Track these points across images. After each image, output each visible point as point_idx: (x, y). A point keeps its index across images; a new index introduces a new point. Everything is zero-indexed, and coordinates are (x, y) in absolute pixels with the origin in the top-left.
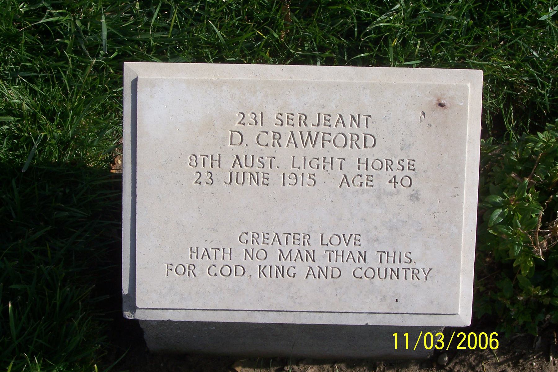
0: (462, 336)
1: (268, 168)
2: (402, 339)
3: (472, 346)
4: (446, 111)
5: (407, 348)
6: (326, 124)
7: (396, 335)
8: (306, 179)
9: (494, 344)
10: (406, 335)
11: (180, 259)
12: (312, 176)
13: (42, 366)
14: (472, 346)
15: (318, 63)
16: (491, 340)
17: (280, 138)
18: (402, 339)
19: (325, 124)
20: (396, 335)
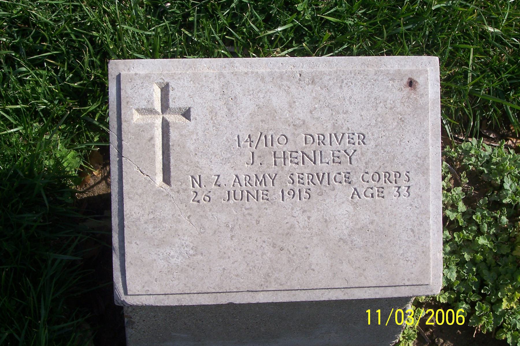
0: (430, 313)
1: (245, 200)
2: (374, 316)
3: (440, 322)
4: (410, 77)
5: (379, 323)
6: (264, 198)
7: (369, 311)
8: (304, 194)
9: (460, 320)
10: (379, 311)
11: (159, 263)
12: (308, 191)
13: (497, 36)
14: (440, 322)
15: (442, 82)
16: (457, 317)
17: (324, 139)
18: (374, 316)
19: (263, 198)
20: (369, 311)
